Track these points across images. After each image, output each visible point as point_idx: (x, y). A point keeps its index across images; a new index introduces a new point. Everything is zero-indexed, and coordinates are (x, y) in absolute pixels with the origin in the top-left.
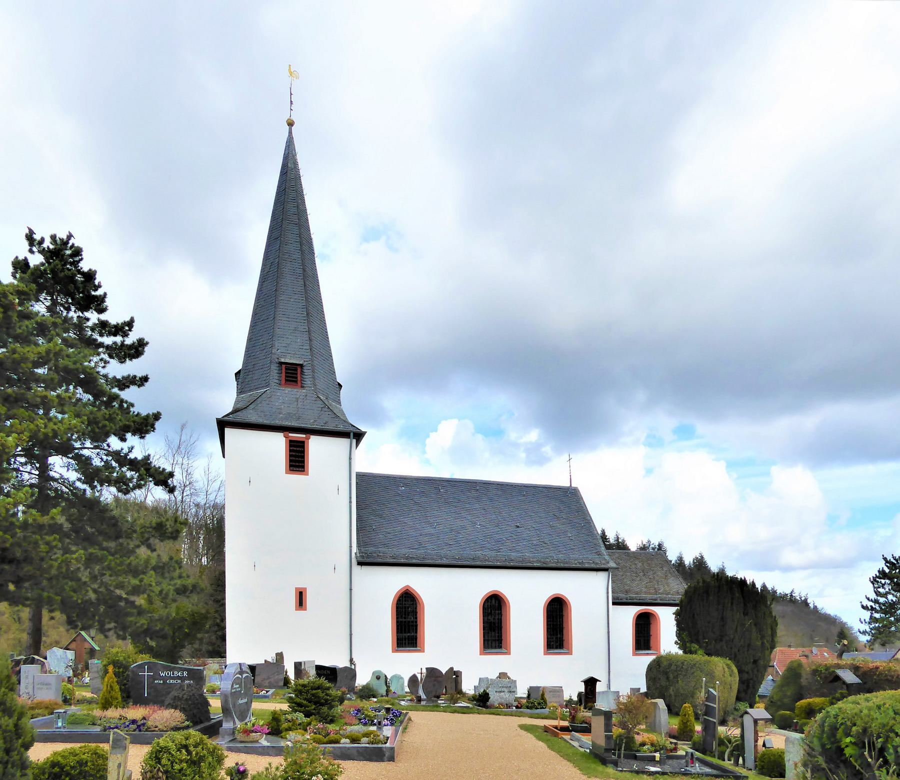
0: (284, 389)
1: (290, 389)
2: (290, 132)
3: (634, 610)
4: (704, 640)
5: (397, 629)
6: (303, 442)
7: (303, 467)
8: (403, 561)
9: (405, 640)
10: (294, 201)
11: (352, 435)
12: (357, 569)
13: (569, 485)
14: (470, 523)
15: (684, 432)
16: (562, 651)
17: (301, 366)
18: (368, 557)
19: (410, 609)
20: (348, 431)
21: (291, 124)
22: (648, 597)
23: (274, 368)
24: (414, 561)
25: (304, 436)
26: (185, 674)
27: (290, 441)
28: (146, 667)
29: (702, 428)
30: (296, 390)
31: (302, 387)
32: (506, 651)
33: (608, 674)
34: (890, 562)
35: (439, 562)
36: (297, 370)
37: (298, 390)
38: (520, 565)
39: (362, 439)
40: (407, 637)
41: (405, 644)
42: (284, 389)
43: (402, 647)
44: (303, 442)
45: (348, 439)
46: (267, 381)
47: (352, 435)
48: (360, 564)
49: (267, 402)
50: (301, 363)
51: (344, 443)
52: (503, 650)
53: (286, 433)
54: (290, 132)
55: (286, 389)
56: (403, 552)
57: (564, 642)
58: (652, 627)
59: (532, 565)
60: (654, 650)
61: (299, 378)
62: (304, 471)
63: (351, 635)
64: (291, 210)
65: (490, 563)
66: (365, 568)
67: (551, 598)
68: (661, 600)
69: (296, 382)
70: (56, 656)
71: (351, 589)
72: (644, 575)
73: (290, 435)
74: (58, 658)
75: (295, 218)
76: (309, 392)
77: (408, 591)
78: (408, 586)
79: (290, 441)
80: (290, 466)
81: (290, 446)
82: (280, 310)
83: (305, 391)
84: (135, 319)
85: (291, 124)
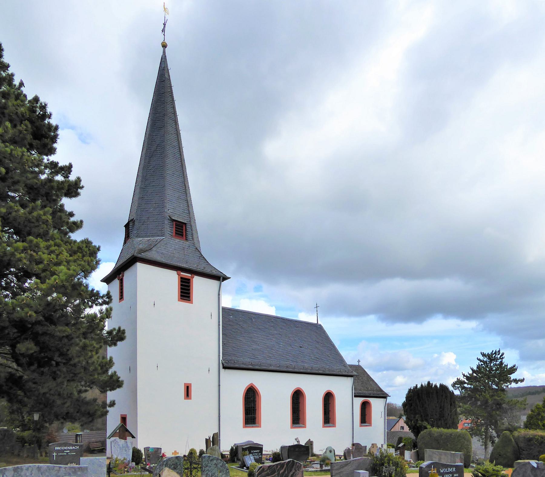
0: (174, 239)
1: (178, 240)
2: (164, 52)
3: (361, 400)
4: (431, 420)
5: (245, 414)
6: (189, 280)
7: (189, 297)
8: (250, 367)
9: (249, 420)
10: (171, 103)
11: (221, 278)
12: (222, 371)
13: (317, 323)
14: (276, 343)
15: (258, 289)
16: (328, 425)
17: (185, 224)
18: (307, 369)
19: (251, 399)
20: (219, 276)
21: (164, 46)
22: (367, 393)
23: (166, 222)
24: (257, 367)
25: (190, 275)
26: (454, 469)
27: (181, 278)
28: (432, 466)
29: (265, 286)
30: (182, 241)
31: (186, 240)
32: (304, 426)
33: (352, 438)
34: (467, 377)
35: (271, 368)
36: (183, 227)
37: (184, 242)
38: (278, 369)
39: (111, 272)
40: (250, 417)
41: (249, 422)
42: (174, 239)
43: (249, 424)
44: (189, 280)
45: (218, 281)
46: (163, 232)
47: (221, 278)
48: (225, 368)
49: (164, 247)
50: (186, 222)
51: (214, 283)
52: (301, 425)
53: (179, 272)
54: (164, 52)
55: (176, 240)
56: (246, 360)
57: (330, 419)
58: (300, 405)
59: (318, 372)
60: (367, 423)
61: (184, 234)
62: (190, 300)
63: (219, 417)
64: (170, 110)
65: (297, 370)
66: (227, 371)
67: (302, 391)
68: (373, 394)
69: (182, 235)
70: (119, 445)
71: (219, 385)
72: (358, 379)
73: (182, 273)
74: (120, 447)
75: (172, 115)
76: (190, 244)
77: (251, 387)
78: (252, 383)
79: (181, 278)
80: (181, 296)
81: (181, 281)
82: (168, 181)
83: (188, 243)
84: (72, 164)
85: (164, 46)
